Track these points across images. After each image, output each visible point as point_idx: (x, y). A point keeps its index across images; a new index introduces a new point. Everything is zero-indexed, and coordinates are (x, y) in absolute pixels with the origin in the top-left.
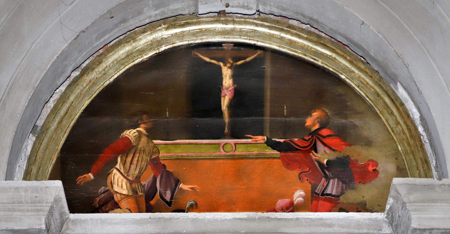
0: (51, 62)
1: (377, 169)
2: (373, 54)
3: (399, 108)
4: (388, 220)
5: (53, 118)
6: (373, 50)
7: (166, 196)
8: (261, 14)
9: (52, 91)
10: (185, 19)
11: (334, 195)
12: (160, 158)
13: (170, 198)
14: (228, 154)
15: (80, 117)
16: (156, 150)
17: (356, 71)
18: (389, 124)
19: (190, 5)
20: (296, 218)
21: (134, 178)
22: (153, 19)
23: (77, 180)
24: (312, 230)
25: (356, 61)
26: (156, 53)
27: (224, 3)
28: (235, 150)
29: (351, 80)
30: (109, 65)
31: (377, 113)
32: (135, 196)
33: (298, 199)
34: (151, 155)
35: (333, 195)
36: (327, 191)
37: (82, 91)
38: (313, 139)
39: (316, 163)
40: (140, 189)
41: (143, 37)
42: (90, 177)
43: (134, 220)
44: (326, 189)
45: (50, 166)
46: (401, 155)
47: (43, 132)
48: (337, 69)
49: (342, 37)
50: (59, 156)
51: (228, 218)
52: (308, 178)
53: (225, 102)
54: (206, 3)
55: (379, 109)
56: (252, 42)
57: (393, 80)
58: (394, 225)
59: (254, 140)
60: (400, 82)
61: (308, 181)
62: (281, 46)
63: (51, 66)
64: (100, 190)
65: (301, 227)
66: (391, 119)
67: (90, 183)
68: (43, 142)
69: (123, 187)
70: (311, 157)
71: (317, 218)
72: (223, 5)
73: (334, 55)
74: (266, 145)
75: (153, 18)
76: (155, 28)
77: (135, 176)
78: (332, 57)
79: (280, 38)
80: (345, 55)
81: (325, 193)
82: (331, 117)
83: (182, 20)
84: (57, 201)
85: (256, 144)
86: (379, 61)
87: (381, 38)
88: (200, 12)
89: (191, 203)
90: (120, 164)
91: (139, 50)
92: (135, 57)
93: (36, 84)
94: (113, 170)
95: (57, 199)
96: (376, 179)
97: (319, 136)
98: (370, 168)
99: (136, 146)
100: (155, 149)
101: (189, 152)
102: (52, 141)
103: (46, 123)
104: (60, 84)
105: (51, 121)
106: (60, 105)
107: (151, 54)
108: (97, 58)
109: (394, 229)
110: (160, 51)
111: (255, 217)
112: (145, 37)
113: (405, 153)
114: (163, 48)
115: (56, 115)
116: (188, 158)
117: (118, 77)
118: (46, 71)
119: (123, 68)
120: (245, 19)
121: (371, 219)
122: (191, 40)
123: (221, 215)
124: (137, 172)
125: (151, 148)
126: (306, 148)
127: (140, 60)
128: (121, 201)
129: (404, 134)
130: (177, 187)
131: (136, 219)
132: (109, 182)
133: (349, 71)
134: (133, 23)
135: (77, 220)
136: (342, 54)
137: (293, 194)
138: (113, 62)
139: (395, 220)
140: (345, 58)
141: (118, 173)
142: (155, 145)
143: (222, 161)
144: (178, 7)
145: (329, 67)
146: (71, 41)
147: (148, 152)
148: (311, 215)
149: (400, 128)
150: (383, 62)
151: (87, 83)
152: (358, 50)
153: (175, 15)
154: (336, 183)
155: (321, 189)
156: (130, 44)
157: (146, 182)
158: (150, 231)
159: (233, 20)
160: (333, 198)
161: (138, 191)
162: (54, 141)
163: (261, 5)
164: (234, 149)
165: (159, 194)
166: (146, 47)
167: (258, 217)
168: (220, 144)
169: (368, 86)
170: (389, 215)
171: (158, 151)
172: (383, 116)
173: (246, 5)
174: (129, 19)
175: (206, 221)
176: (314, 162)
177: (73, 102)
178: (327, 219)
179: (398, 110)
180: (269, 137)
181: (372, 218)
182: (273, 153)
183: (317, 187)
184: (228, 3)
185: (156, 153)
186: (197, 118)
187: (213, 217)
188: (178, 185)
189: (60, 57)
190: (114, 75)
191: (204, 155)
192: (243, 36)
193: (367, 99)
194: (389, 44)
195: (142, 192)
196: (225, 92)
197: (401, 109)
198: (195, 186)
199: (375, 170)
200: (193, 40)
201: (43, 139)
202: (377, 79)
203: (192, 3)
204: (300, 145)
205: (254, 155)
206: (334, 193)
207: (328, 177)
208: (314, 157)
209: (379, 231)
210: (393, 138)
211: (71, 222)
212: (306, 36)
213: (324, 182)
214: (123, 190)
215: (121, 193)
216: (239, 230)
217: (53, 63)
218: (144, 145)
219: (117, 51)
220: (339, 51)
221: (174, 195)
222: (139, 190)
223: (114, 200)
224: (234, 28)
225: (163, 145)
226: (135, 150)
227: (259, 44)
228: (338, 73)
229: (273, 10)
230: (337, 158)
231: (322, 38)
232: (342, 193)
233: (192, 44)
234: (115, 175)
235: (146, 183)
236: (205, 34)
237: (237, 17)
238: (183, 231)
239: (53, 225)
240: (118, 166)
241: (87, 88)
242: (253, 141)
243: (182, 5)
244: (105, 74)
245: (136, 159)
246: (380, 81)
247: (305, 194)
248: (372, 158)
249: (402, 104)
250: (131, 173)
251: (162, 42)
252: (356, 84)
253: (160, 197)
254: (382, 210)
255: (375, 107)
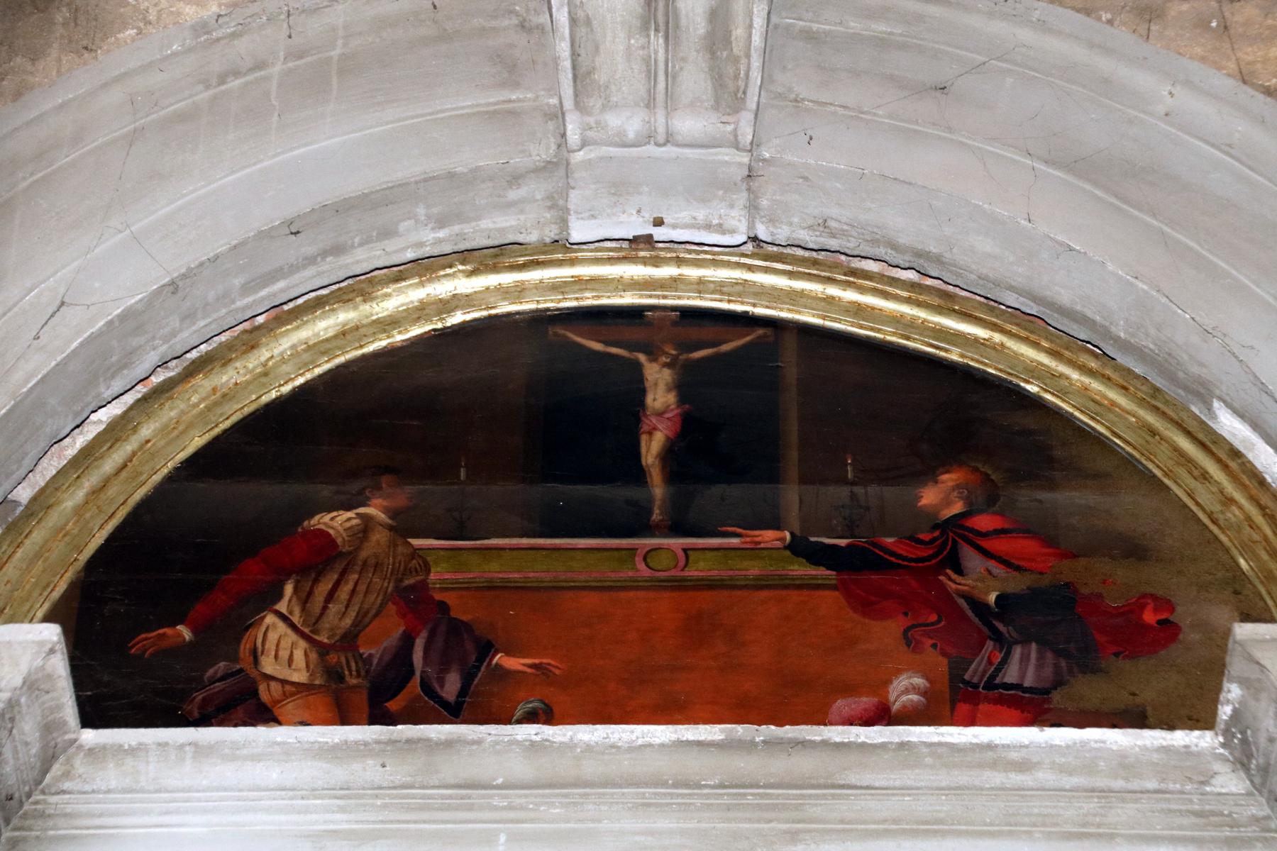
0: (86, 335)
1: (1171, 618)
2: (1125, 333)
3: (1228, 461)
4: (1231, 754)
5: (72, 479)
6: (1122, 323)
7: (442, 686)
8: (762, 244)
9: (83, 410)
10: (527, 252)
11: (1031, 688)
12: (430, 586)
13: (457, 693)
14: (662, 575)
15: (169, 479)
16: (419, 564)
17: (1075, 375)
18: (1198, 504)
19: (543, 219)
20: (897, 743)
21: (337, 638)
22: (428, 251)
23: (133, 642)
24: (960, 778)
25: (1070, 351)
26: (434, 330)
27: (649, 216)
28: (686, 565)
29: (1058, 397)
30: (282, 354)
31: (1154, 476)
32: (334, 686)
33: (904, 698)
34: (400, 576)
35: (1026, 688)
36: (1003, 677)
37: (183, 412)
38: (947, 539)
39: (962, 602)
40: (354, 668)
41: (394, 291)
42: (180, 635)
43: (317, 746)
44: (1000, 671)
45: (41, 606)
46: (1250, 583)
47: (32, 515)
48: (1012, 369)
49: (1020, 295)
50: (77, 578)
51: (657, 741)
52: (934, 641)
53: (652, 447)
54: (593, 217)
55: (1158, 467)
56: (739, 308)
57: (1198, 395)
58: (1253, 766)
59: (748, 539)
60: (1221, 399)
61: (936, 649)
62: (829, 317)
63: (82, 344)
64: (211, 671)
65: (917, 771)
66: (1203, 492)
67: (181, 650)
68: (27, 542)
69: (294, 663)
70: (942, 587)
71: (974, 744)
72: (645, 222)
73: (997, 337)
74: (788, 553)
75: (428, 248)
76: (435, 271)
77: (340, 632)
78: (991, 343)
79: (824, 299)
80: (1032, 337)
81: (996, 682)
82: (1000, 485)
83: (518, 254)
84: (33, 685)
85: (754, 551)
86: (1146, 350)
87: (1143, 290)
88: (576, 236)
89: (530, 706)
90: (290, 601)
91: (382, 320)
92: (365, 336)
93: (24, 386)
94: (263, 618)
95: (37, 680)
96: (1173, 646)
97: (966, 533)
98: (1149, 617)
99: (350, 553)
100: (414, 561)
101: (530, 570)
102: (58, 539)
103: (48, 492)
104: (114, 396)
105: (64, 487)
106: (101, 447)
107: (416, 331)
108: (245, 337)
109: (1257, 780)
110: (448, 324)
111: (754, 737)
112: (400, 291)
113: (1265, 577)
114: (457, 318)
115: (86, 472)
116: (529, 585)
117: (307, 383)
118: (64, 355)
119: (327, 362)
120: (714, 255)
121: (1170, 750)
122: (546, 301)
123: (632, 732)
124: (348, 622)
125: (403, 560)
126: (923, 563)
127: (383, 343)
128: (283, 700)
129: (1252, 528)
130: (485, 664)
131: (327, 743)
132: (245, 649)
133: (1049, 375)
134: (362, 259)
135: (108, 747)
136: (1023, 333)
137: (888, 682)
138: (293, 347)
139: (1258, 750)
140: (1036, 345)
141: (282, 627)
142: (415, 552)
143: (640, 594)
144: (508, 224)
145: (986, 364)
146: (158, 288)
147: (390, 570)
148: (951, 735)
149: (1237, 512)
150: (1160, 351)
151: (204, 395)
152: (1075, 327)
153: (497, 243)
154: (1033, 655)
155: (985, 672)
156: (352, 306)
157: (376, 649)
158: (373, 781)
159: (678, 257)
160: (1027, 695)
161: (347, 673)
162: (67, 539)
163: (760, 224)
164: (682, 563)
165: (419, 681)
166: (404, 315)
167: (762, 738)
168: (637, 549)
169: (1117, 409)
170: (1234, 736)
171: (425, 566)
172: (1176, 482)
173: (715, 222)
174: (353, 247)
175: (579, 750)
176: (953, 598)
177: (148, 442)
178: (1008, 746)
179: (1225, 467)
180: (798, 532)
181: (1173, 746)
182: (814, 573)
183: (970, 665)
184: (662, 218)
185: (416, 571)
186: (561, 483)
187: (604, 738)
188: (488, 655)
189: (117, 324)
190: (296, 377)
191: (582, 577)
192: (708, 294)
193: (1118, 441)
194: (1170, 304)
195: (358, 675)
196: (651, 421)
197: (1233, 465)
198: (545, 661)
199: (1164, 623)
200: (552, 301)
201: (30, 531)
202: (1146, 393)
203: (548, 215)
204: (905, 554)
205: (750, 580)
206: (1028, 683)
207: (1006, 638)
208: (954, 586)
209: (1202, 786)
210: (1216, 538)
211: (85, 755)
212: (905, 294)
213: (991, 652)
214: (294, 670)
215: (286, 678)
216: (697, 778)
217: (89, 337)
218: (380, 551)
219: (307, 321)
220: (1014, 329)
221: (472, 684)
222: (350, 671)
223: (259, 699)
224: (680, 275)
225: (442, 553)
226: (348, 564)
227: (760, 311)
228: (1015, 380)
229: (801, 237)
230: (1028, 588)
231: (956, 299)
232: (1058, 683)
233: (548, 309)
234: (270, 631)
235: (377, 651)
236: (588, 287)
237: (690, 252)
238: (495, 780)
239: (11, 762)
240: (282, 607)
241: (202, 406)
242: (746, 543)
243: (519, 219)
244: (266, 374)
245: (346, 588)
246: (1153, 397)
247: (928, 685)
248: (1150, 590)
249: (1236, 454)
250: (327, 626)
251: (453, 304)
252: (1078, 406)
253: (423, 690)
254: (1201, 719)
255: (1145, 462)
